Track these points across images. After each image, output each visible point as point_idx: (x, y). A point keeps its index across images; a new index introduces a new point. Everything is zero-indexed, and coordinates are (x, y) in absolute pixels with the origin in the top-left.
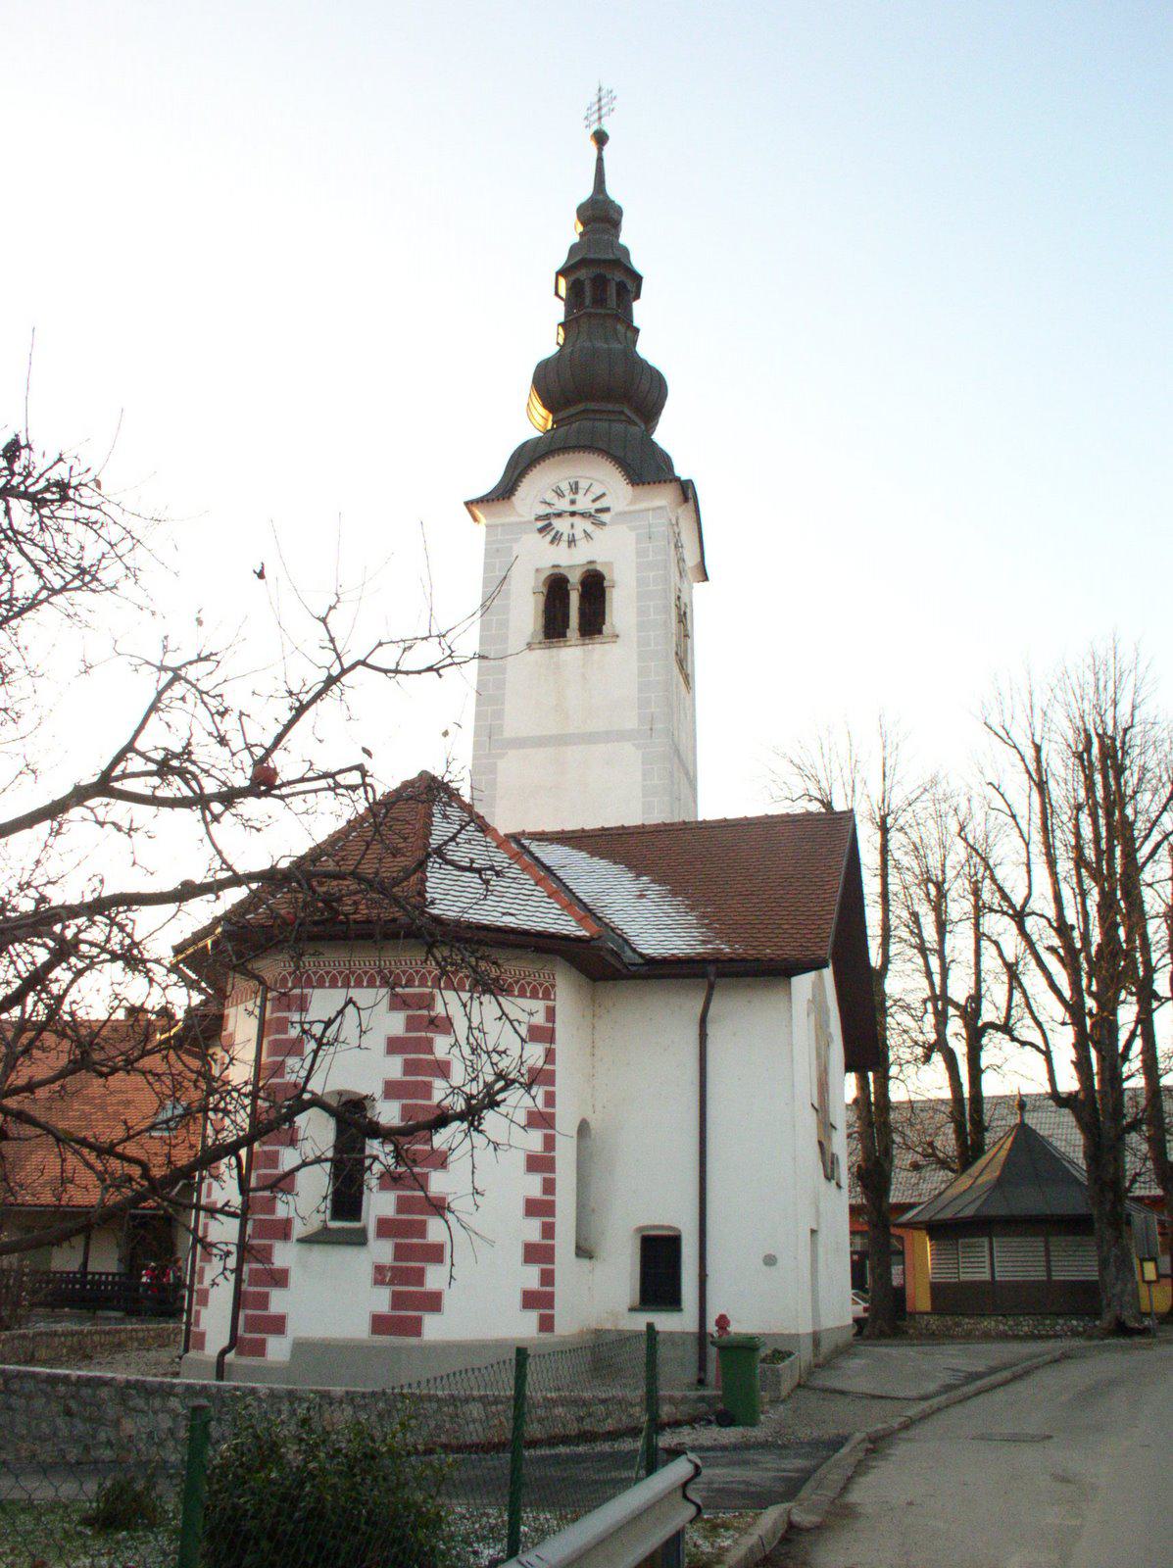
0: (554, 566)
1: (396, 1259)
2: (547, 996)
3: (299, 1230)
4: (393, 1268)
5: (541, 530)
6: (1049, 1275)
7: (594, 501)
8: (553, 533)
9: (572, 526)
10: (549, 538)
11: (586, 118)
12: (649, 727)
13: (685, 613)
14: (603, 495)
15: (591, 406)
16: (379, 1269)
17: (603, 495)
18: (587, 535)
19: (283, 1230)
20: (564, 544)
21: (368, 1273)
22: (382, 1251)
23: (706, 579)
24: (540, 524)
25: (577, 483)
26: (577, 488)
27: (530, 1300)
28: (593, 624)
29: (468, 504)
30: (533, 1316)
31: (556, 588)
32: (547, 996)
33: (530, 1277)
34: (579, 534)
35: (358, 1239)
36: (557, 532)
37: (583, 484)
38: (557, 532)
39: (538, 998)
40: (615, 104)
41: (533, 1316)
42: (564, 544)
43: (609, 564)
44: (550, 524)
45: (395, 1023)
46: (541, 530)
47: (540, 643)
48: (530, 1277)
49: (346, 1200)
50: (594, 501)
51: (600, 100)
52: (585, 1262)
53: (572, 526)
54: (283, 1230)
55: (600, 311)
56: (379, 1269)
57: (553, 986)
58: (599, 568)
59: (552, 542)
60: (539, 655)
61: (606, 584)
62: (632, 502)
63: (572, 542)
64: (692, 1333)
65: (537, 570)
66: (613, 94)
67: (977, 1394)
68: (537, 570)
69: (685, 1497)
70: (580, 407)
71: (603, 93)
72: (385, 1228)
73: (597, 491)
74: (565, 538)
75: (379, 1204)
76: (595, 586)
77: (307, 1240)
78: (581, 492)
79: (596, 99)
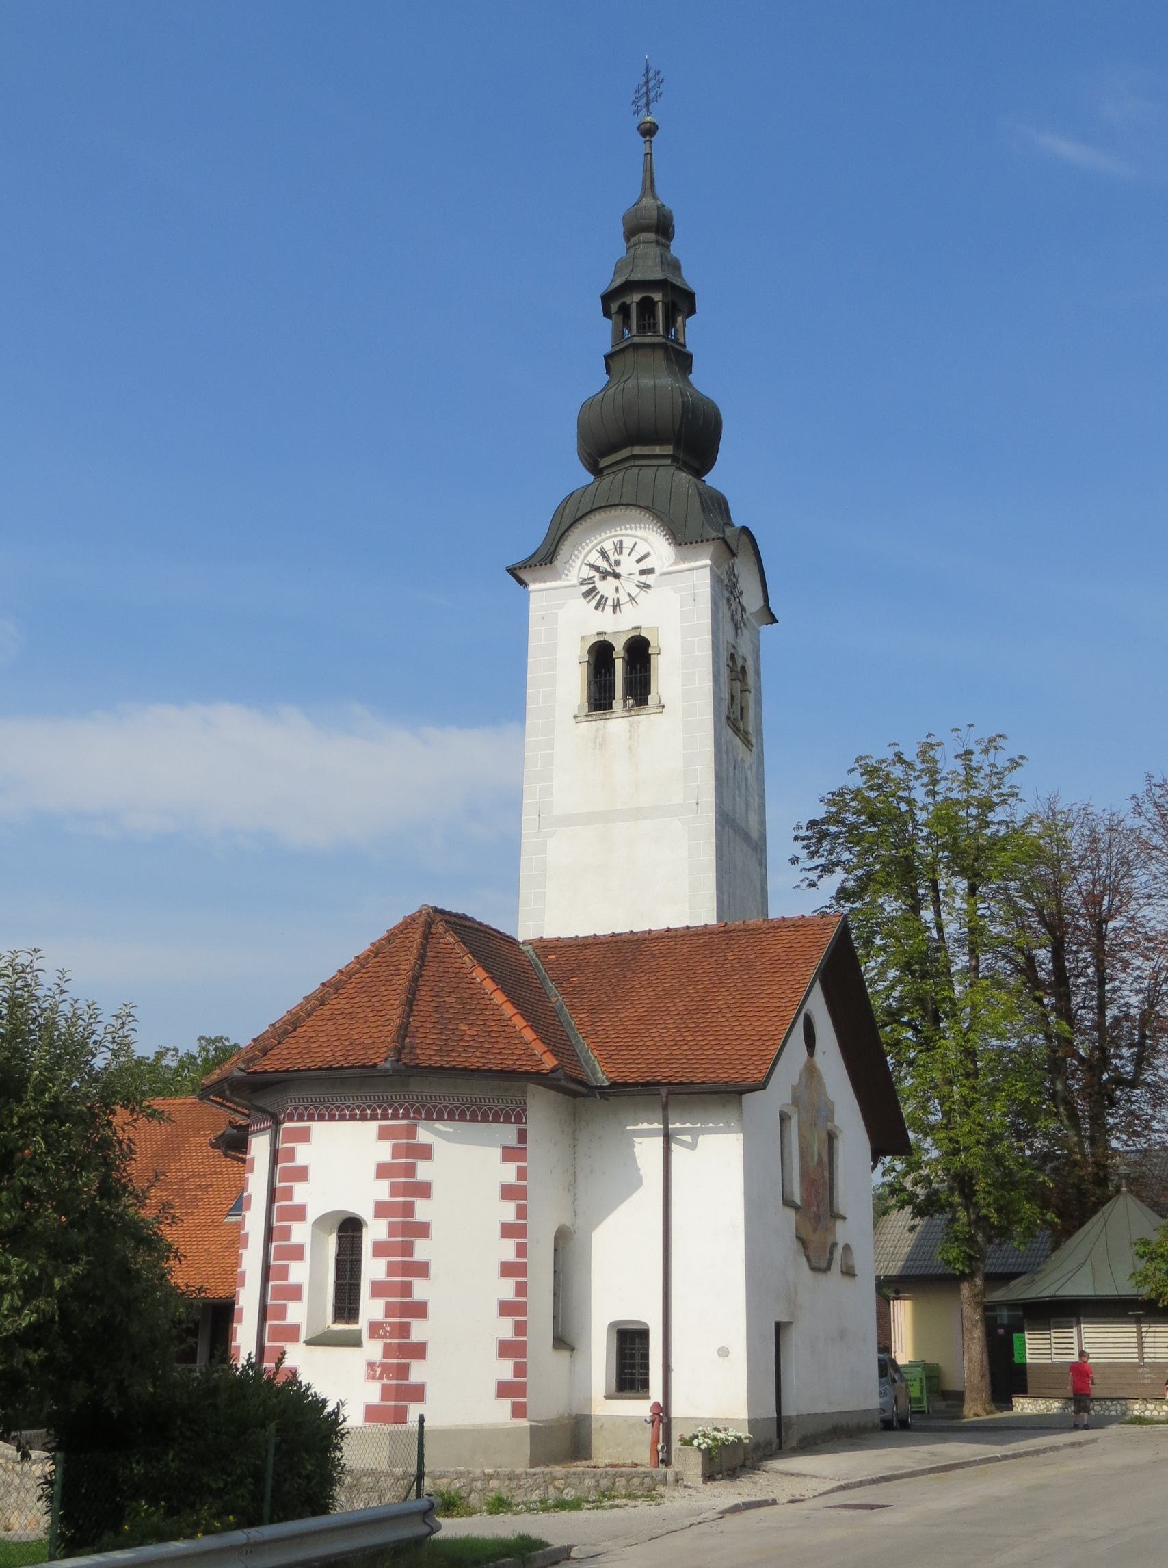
0: (599, 634)
1: (385, 1357)
2: (519, 1120)
3: (303, 1336)
4: (382, 1365)
5: (586, 594)
6: (1140, 1332)
7: (638, 561)
8: (598, 598)
9: (617, 589)
10: (594, 602)
11: (634, 102)
12: (695, 801)
13: (743, 668)
14: (647, 555)
15: (637, 450)
16: (371, 1365)
17: (647, 555)
18: (632, 599)
19: (292, 1333)
20: (609, 609)
21: (363, 1370)
22: (373, 1350)
23: (775, 621)
24: (585, 588)
25: (621, 542)
26: (621, 548)
27: (504, 1390)
28: (639, 690)
29: (512, 571)
30: (507, 1404)
31: (601, 655)
32: (519, 1120)
33: (505, 1370)
34: (624, 598)
35: (353, 1341)
36: (602, 597)
37: (627, 543)
38: (602, 597)
39: (511, 1123)
40: (663, 87)
41: (507, 1404)
42: (609, 609)
43: (655, 630)
44: (594, 589)
45: (384, 1152)
46: (586, 594)
47: (587, 716)
48: (505, 1370)
49: (346, 1306)
50: (638, 561)
51: (647, 82)
52: (564, 1355)
53: (617, 589)
54: (292, 1333)
55: (648, 340)
56: (371, 1365)
57: (525, 1111)
58: (644, 634)
59: (597, 608)
60: (589, 728)
61: (651, 651)
62: (675, 563)
63: (617, 606)
64: (591, 1412)
65: (583, 638)
66: (661, 76)
67: (1014, 1456)
68: (583, 638)
69: (432, 1528)
70: (625, 453)
71: (651, 74)
72: (375, 1329)
73: (640, 551)
74: (610, 602)
75: (371, 1309)
76: (639, 650)
77: (309, 1343)
78: (626, 552)
79: (644, 79)
